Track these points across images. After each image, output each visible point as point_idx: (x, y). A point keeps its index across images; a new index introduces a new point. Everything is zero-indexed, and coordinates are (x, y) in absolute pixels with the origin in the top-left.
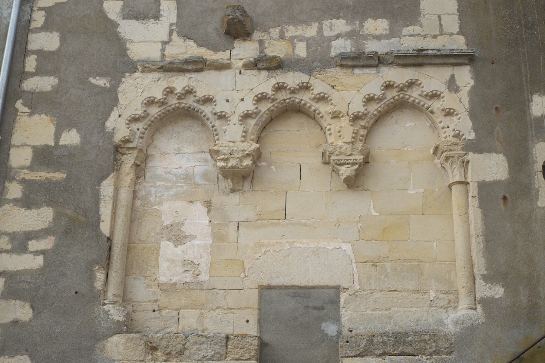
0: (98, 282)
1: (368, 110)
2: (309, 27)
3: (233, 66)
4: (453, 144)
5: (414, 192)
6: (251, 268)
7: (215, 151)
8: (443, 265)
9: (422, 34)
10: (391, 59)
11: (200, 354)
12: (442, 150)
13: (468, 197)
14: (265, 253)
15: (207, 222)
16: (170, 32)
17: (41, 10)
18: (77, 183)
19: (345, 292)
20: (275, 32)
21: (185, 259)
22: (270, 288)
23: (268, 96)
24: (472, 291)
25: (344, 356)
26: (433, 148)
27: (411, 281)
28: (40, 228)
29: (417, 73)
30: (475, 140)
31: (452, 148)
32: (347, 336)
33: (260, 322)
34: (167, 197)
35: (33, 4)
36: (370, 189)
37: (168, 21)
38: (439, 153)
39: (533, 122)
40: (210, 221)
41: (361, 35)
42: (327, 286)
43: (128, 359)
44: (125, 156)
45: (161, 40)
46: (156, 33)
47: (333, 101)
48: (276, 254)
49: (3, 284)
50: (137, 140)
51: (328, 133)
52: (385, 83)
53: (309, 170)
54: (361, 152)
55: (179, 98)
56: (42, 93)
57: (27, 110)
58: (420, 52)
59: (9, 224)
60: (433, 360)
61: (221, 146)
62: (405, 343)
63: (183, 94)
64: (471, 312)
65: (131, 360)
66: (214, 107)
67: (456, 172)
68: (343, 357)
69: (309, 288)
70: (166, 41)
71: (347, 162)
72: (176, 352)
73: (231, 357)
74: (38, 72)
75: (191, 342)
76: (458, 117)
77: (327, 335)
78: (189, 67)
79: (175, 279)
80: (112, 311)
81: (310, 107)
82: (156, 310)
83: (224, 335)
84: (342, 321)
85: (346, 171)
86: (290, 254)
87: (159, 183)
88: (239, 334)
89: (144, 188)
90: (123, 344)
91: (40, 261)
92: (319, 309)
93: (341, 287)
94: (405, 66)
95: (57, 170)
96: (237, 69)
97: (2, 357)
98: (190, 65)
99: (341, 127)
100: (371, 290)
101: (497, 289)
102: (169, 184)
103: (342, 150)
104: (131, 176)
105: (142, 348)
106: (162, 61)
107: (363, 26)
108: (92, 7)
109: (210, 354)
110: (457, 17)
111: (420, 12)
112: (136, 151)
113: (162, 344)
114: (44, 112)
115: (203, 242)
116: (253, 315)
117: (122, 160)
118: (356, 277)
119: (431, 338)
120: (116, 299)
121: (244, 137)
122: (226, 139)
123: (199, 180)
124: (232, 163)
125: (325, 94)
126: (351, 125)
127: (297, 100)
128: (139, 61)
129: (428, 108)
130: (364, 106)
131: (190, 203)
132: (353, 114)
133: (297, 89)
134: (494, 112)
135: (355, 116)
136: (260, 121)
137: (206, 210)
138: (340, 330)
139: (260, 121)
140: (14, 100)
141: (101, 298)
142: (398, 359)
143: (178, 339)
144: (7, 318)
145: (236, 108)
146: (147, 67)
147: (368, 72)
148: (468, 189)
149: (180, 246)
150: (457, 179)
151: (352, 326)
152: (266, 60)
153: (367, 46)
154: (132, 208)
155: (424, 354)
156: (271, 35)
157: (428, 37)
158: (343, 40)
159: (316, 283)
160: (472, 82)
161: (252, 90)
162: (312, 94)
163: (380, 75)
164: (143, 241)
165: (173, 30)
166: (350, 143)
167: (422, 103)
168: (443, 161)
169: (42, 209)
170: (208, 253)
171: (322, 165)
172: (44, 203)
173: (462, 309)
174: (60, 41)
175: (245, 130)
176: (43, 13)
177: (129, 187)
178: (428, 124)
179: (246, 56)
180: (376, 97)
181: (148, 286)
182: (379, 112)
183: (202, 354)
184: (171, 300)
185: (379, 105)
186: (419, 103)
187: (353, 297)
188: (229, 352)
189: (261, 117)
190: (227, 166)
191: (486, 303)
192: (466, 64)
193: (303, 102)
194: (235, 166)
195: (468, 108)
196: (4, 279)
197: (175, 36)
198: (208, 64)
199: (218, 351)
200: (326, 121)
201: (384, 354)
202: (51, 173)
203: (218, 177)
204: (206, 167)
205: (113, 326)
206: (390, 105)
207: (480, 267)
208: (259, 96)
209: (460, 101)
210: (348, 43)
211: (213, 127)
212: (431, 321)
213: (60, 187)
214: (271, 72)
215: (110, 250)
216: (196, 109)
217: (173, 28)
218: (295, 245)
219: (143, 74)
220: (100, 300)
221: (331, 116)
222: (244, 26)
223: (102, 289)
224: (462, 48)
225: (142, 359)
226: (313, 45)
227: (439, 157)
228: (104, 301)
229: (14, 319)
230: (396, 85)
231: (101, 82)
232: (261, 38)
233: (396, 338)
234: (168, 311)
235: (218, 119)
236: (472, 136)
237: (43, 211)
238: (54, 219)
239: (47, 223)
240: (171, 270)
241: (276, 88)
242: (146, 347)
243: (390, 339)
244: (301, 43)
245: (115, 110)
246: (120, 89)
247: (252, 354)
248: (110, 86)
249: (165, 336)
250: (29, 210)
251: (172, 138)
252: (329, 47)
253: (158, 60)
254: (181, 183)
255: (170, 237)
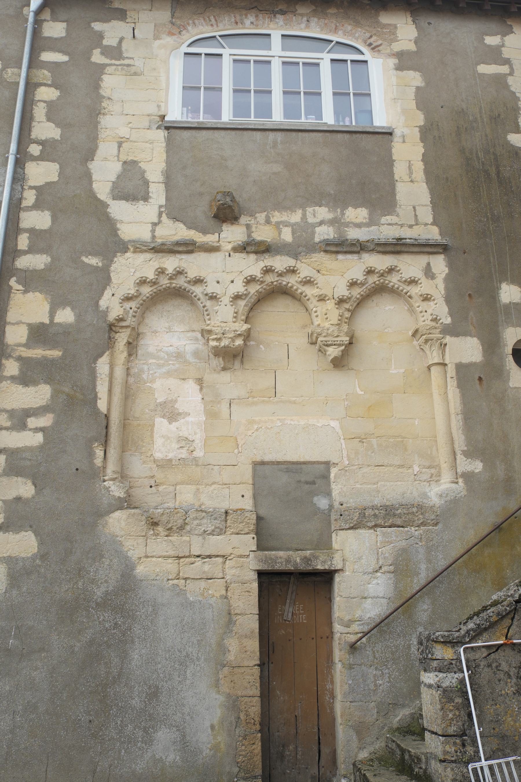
0: (97, 459)
1: (352, 294)
2: (293, 213)
3: (222, 248)
4: (431, 328)
5: (396, 372)
6: (244, 444)
7: (208, 330)
8: (425, 441)
9: (399, 223)
10: (372, 247)
11: (200, 529)
12: (422, 334)
13: (446, 377)
14: (257, 430)
15: (200, 399)
16: (159, 214)
17: (32, 189)
18: (73, 361)
19: (335, 467)
20: (261, 217)
21: (180, 436)
22: (263, 463)
23: (257, 279)
24: (454, 466)
25: (339, 528)
26: (412, 331)
27: (396, 456)
28: (38, 405)
29: (396, 260)
30: (451, 324)
31: (431, 331)
32: (341, 510)
33: (255, 497)
34: (160, 374)
35: (24, 183)
36: (355, 369)
37: (157, 203)
38: (418, 336)
39: (502, 309)
40: (203, 399)
41: (343, 223)
42: (317, 461)
43: (130, 535)
44: (118, 334)
45: (151, 222)
46: (146, 215)
47: (318, 285)
48: (268, 431)
49: (5, 461)
50: (130, 319)
51: (314, 315)
52: (367, 269)
53: (296, 349)
54: (347, 334)
55: (171, 278)
56: (36, 270)
57: (20, 287)
58: (399, 241)
59: (7, 402)
60: (421, 531)
61: (213, 326)
62: (395, 515)
63: (174, 275)
64: (454, 486)
65: (133, 536)
66: (205, 288)
67: (435, 354)
68: (338, 530)
69: (301, 464)
70: (155, 223)
71: (334, 343)
72: (177, 527)
73: (230, 531)
74: (31, 250)
75: (191, 517)
76: (435, 302)
77: (319, 509)
78: (180, 249)
79: (170, 456)
80: (113, 488)
81: (296, 290)
82: (153, 485)
83: (223, 510)
84: (333, 495)
85: (333, 352)
86: (281, 430)
87: (151, 361)
88: (238, 509)
89: (137, 365)
90: (125, 520)
91: (39, 438)
92: (310, 484)
93: (331, 463)
94: (385, 253)
95: (53, 348)
96: (226, 251)
97: (7, 533)
98: (181, 247)
99: (327, 310)
100: (359, 465)
101: (476, 464)
102: (161, 362)
103: (329, 331)
104: (125, 354)
105: (143, 524)
106: (152, 242)
107: (344, 214)
108: (82, 187)
109: (210, 528)
110: (430, 208)
111: (397, 203)
112: (129, 330)
113: (163, 519)
114: (38, 290)
115: (197, 419)
116: (248, 490)
117: (116, 338)
118: (345, 455)
119: (418, 511)
120: (115, 476)
121: (235, 317)
122: (218, 320)
123: (190, 358)
124: (224, 343)
125: (311, 277)
126: (337, 308)
127: (284, 283)
128: (130, 241)
129: (406, 293)
130: (348, 290)
131: (182, 381)
132: (338, 298)
133: (285, 273)
134: (467, 298)
135: (340, 299)
136: (250, 302)
137: (199, 387)
138: (331, 504)
139: (250, 302)
140: (8, 278)
141: (101, 475)
142: (389, 530)
143: (178, 515)
144: (11, 495)
145: (227, 289)
146: (138, 248)
147: (351, 258)
148: (446, 370)
149: (174, 423)
150: (436, 361)
151: (343, 500)
152: (255, 244)
153: (348, 233)
154: (127, 386)
155: (412, 526)
156: (258, 219)
157: (404, 226)
158: (326, 227)
159: (307, 458)
160: (447, 270)
161: (241, 272)
162: (299, 277)
163: (362, 261)
164: (138, 418)
165: (162, 212)
166: (337, 325)
167: (401, 288)
168: (422, 343)
169: (40, 386)
170: (202, 430)
171: (309, 345)
172: (41, 381)
173: (445, 483)
174: (51, 220)
175: (236, 310)
176: (34, 192)
177: (123, 364)
178: (406, 308)
179: (235, 240)
180: (359, 282)
181: (144, 462)
182: (362, 295)
183: (203, 529)
184: (168, 476)
185: (362, 289)
186: (398, 288)
187: (343, 471)
188: (229, 526)
189: (250, 298)
190: (220, 345)
191: (468, 477)
192: (441, 253)
193: (290, 285)
194: (228, 346)
195: (444, 294)
196: (5, 456)
197: (164, 217)
198: (198, 246)
199: (218, 525)
200: (313, 304)
201: (376, 526)
202: (47, 351)
203: (209, 356)
204: (197, 345)
205: (114, 502)
206: (372, 289)
207: (460, 443)
208: (249, 278)
209: (436, 287)
210: (331, 229)
211: (204, 307)
212: (416, 494)
213: (57, 364)
214: (259, 255)
215: (107, 427)
216: (187, 290)
217: (163, 209)
218: (286, 422)
219: (135, 254)
220: (101, 477)
221: (317, 299)
222: (233, 210)
223: (102, 466)
224: (437, 238)
225: (144, 534)
226: (298, 231)
227: (417, 339)
228: (104, 478)
229: (17, 496)
230: (376, 271)
231: (94, 261)
232: (248, 222)
233: (386, 511)
234: (164, 487)
235: (209, 299)
236: (449, 320)
237: (41, 389)
238: (52, 396)
239: (46, 400)
240: (166, 446)
241: (264, 271)
242: (148, 522)
243: (381, 512)
244: (286, 228)
245: (108, 289)
246: (112, 268)
247: (251, 528)
248: (103, 265)
249: (165, 512)
250: (27, 388)
251: (162, 316)
252: (313, 233)
253: (149, 241)
254: (173, 361)
255: (164, 414)
